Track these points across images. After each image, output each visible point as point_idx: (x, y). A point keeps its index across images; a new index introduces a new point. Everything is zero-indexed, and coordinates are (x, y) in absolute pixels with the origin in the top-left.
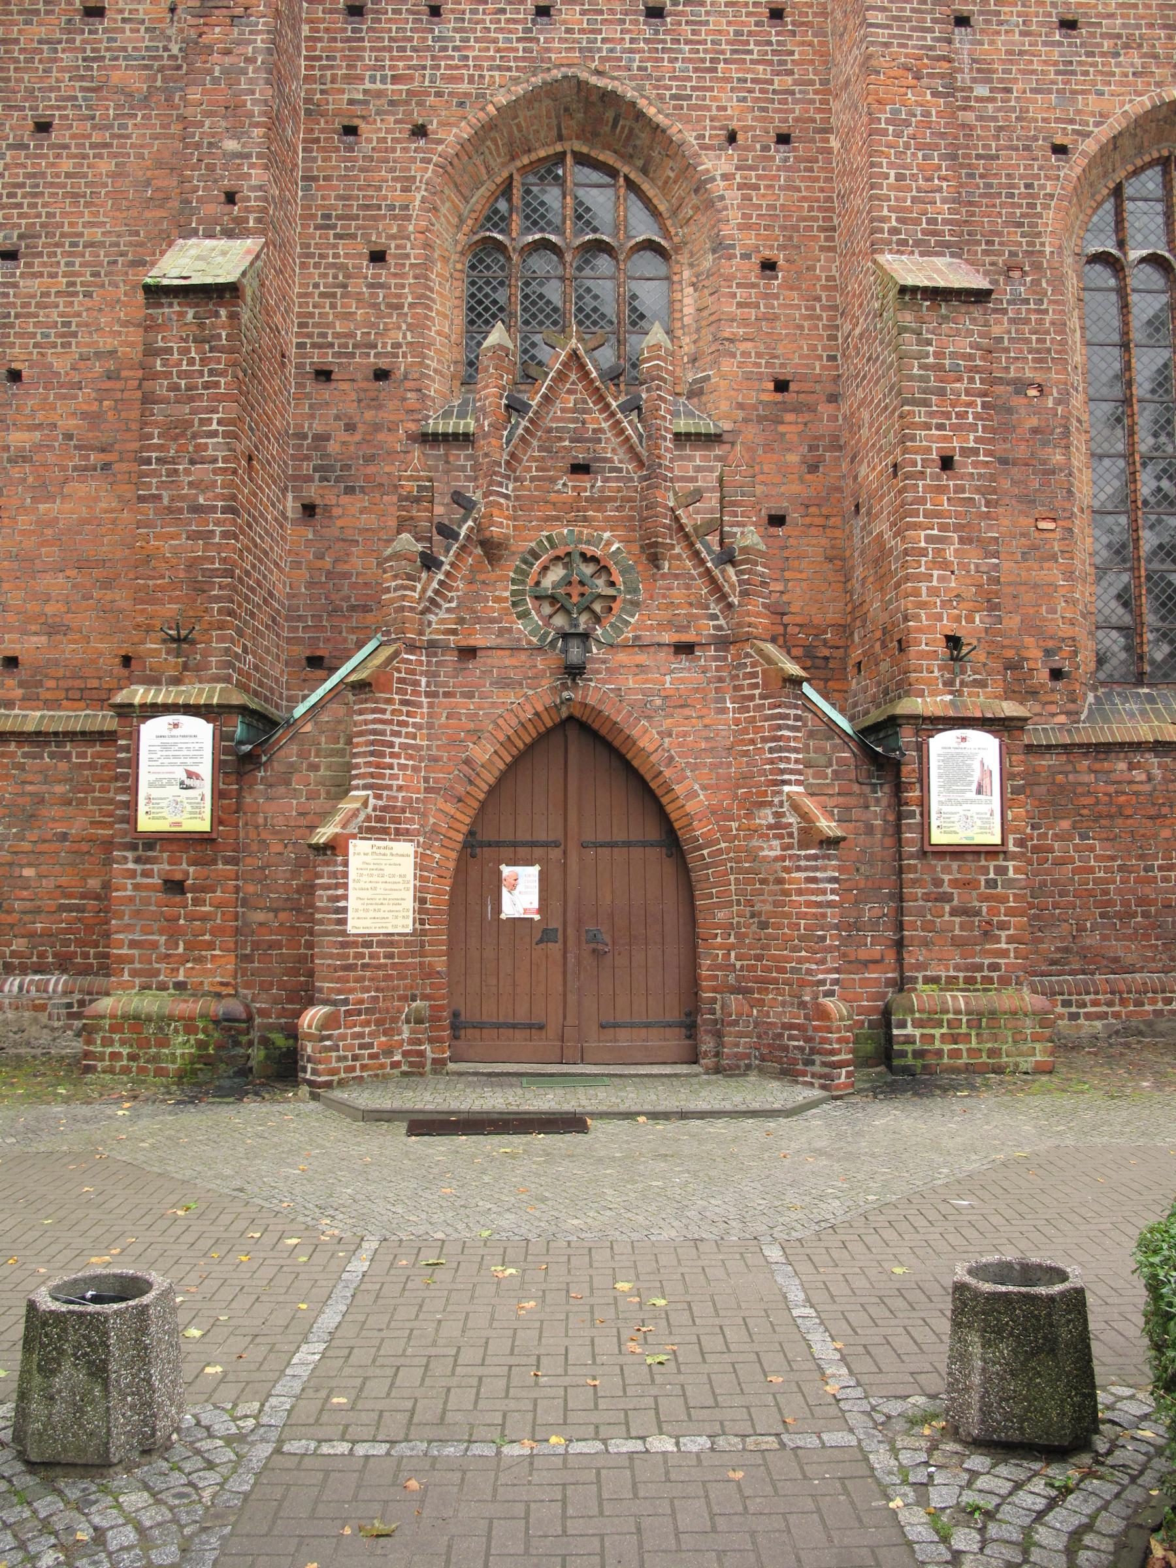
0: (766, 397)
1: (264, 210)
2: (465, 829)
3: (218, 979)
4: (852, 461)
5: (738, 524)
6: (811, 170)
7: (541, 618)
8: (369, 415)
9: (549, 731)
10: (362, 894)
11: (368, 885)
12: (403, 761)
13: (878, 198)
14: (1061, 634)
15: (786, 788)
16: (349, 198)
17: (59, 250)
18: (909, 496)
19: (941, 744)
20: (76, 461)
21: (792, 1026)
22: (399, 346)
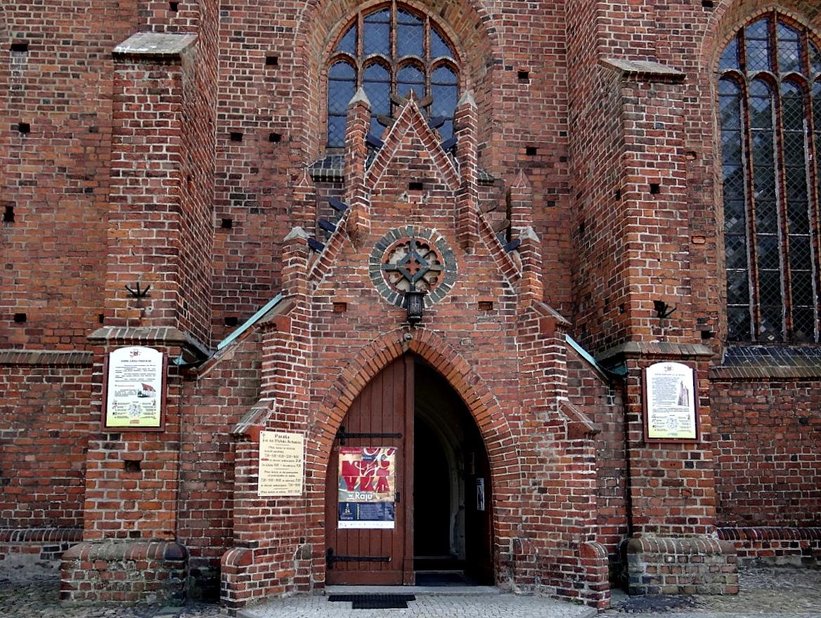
0: (521, 158)
1: (197, 15)
2: (338, 425)
3: (163, 529)
4: (578, 197)
5: (521, 225)
6: (550, 13)
7: (390, 284)
8: (267, 163)
9: (395, 360)
10: (270, 469)
11: (273, 463)
12: (296, 378)
13: (603, 21)
14: (708, 310)
15: (558, 398)
16: (252, 22)
17: (56, 46)
18: (631, 210)
19: (655, 372)
20: (68, 186)
21: (567, 561)
22: (286, 119)
